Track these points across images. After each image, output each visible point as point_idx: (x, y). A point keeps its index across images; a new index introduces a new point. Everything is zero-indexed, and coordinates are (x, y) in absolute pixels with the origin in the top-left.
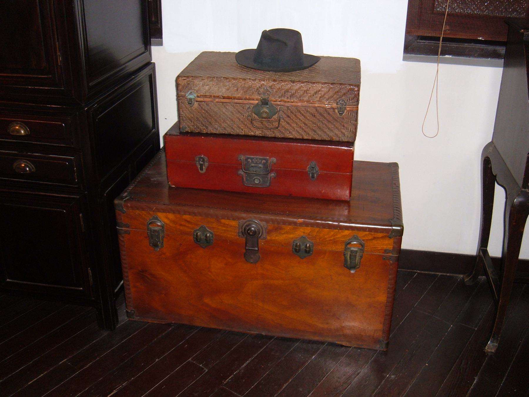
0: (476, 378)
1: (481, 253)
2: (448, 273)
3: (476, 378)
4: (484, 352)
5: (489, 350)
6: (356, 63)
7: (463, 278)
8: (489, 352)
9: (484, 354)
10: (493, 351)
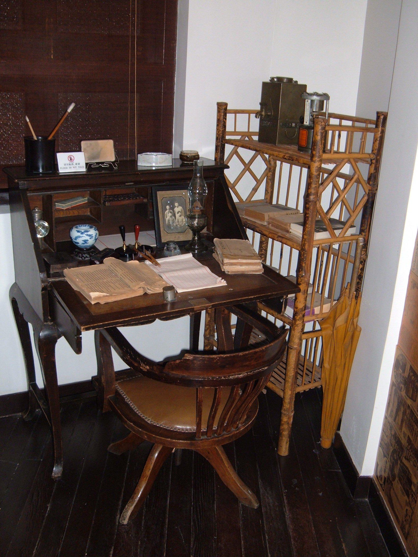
0: (49, 505)
1: (31, 388)
2: (6, 415)
3: (49, 505)
4: (53, 479)
5: (56, 476)
6: (265, 85)
7: (22, 416)
8: (57, 477)
9: (52, 481)
10: (60, 475)
